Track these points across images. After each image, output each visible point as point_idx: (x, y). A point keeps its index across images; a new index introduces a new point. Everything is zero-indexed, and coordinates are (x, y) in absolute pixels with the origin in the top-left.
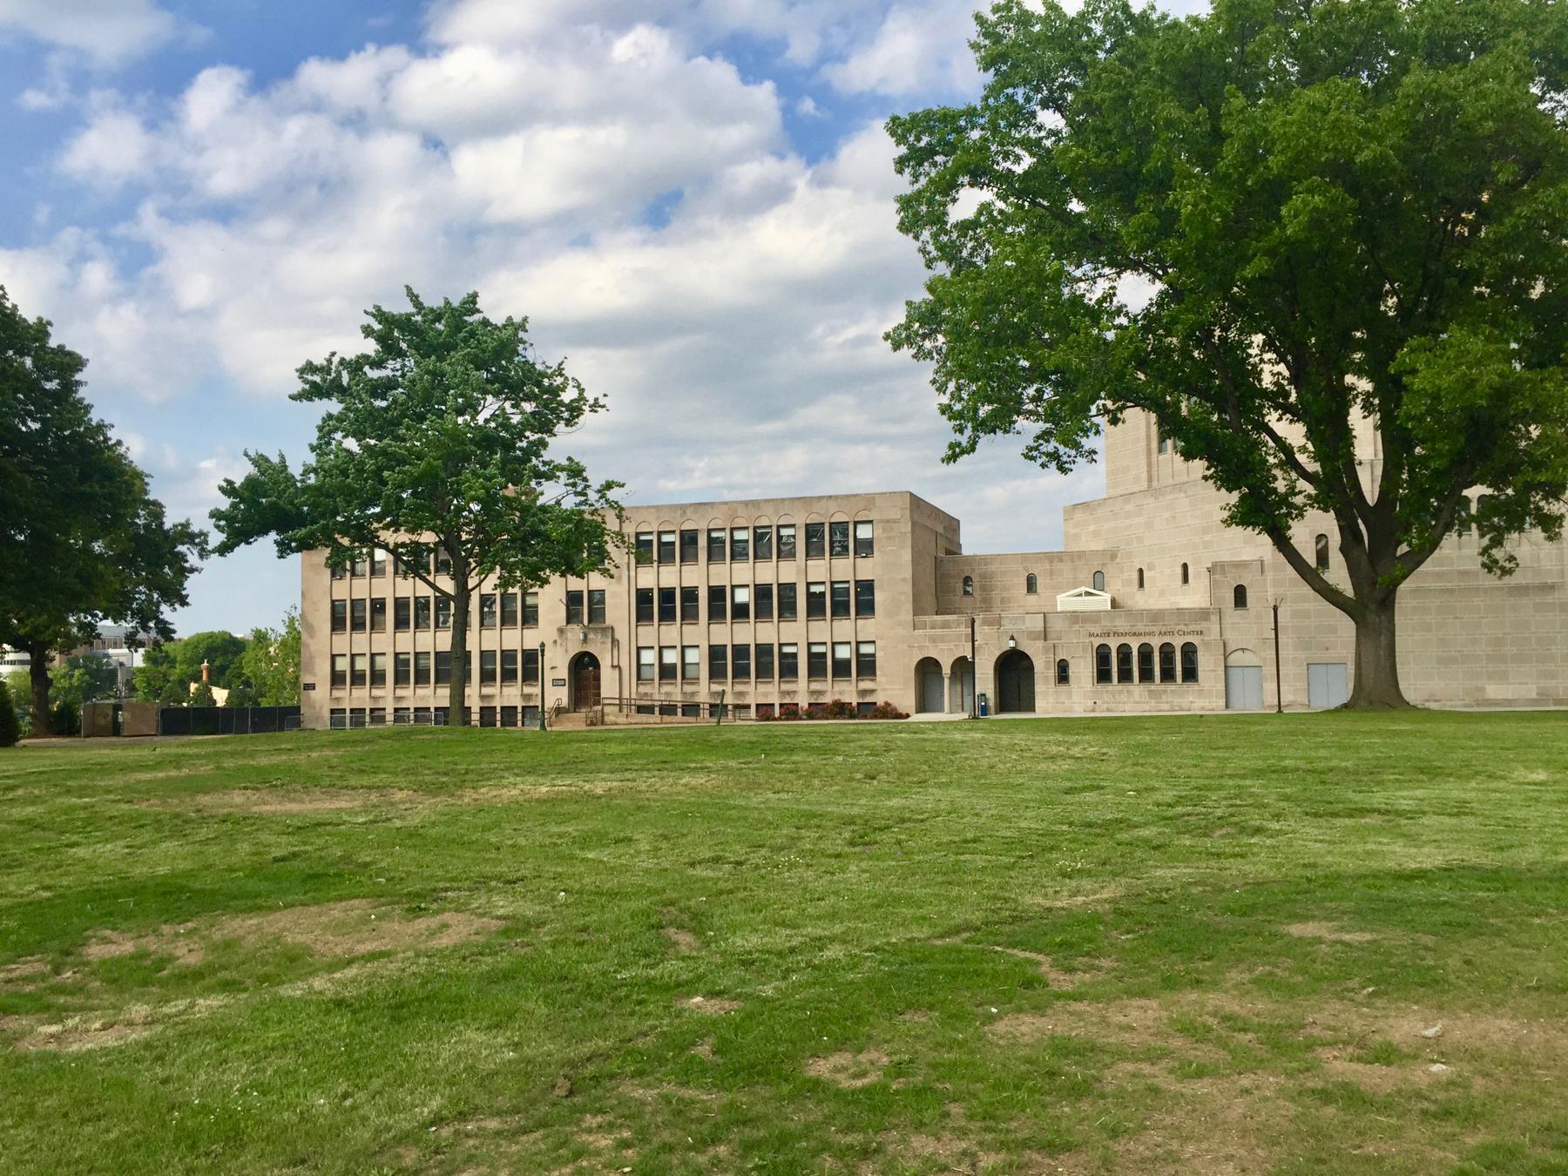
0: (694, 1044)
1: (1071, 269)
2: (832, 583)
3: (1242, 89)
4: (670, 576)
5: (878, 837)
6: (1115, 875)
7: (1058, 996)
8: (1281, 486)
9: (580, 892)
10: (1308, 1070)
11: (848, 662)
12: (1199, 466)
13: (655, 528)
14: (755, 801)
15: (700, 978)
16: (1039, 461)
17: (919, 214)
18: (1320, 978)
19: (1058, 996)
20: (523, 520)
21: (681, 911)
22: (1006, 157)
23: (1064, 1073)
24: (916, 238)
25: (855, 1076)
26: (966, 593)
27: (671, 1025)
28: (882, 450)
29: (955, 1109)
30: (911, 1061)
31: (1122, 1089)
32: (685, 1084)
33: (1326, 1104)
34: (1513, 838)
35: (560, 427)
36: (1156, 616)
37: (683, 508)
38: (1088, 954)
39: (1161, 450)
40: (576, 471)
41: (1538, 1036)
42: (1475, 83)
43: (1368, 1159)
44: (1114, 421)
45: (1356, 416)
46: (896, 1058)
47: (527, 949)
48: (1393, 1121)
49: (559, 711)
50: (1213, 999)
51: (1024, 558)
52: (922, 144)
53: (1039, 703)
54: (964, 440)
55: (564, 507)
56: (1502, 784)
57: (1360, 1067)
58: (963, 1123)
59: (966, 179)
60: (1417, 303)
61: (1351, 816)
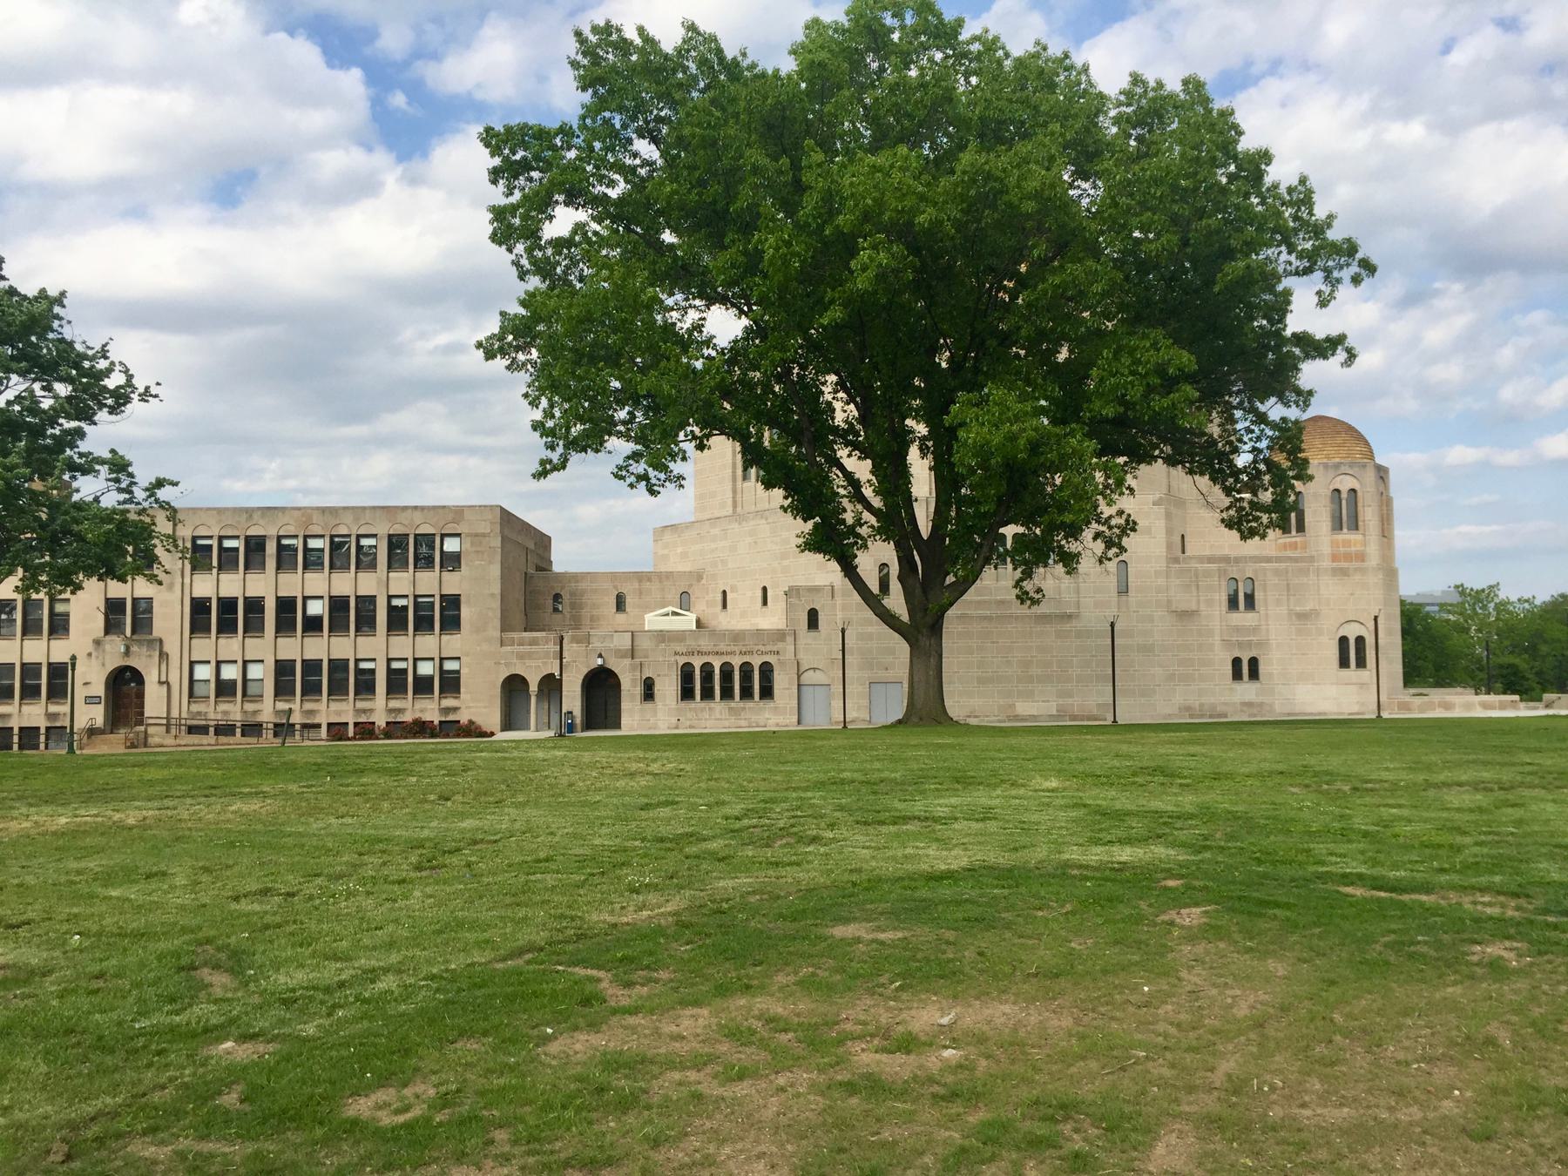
0: (220, 1093)
1: (663, 297)
2: (416, 597)
3: (820, 145)
4: (232, 585)
5: (448, 860)
6: (680, 888)
7: (615, 1012)
8: (849, 517)
9: (99, 934)
10: (838, 1064)
11: (431, 678)
12: (778, 494)
13: (215, 532)
14: (315, 826)
15: (232, 1021)
16: (629, 481)
17: (510, 228)
18: (856, 976)
19: (615, 1012)
20: (52, 519)
21: (219, 949)
22: (601, 178)
23: (610, 1090)
24: (510, 250)
25: (398, 1112)
26: (556, 610)
27: (194, 1074)
28: (473, 462)
29: (500, 1135)
30: (458, 1091)
31: (667, 1098)
32: (202, 1138)
33: (851, 1095)
34: (1024, 840)
35: (103, 415)
36: (737, 636)
37: (249, 512)
38: (648, 967)
39: (745, 478)
40: (119, 466)
41: (1034, 1019)
42: (1019, 166)
43: (883, 1144)
44: (701, 447)
45: (914, 453)
46: (443, 1089)
47: (28, 1002)
48: (908, 1106)
49: (92, 732)
50: (761, 1003)
51: (614, 576)
52: (518, 157)
53: (624, 720)
54: (555, 457)
55: (103, 505)
56: (1022, 791)
57: (884, 1057)
58: (507, 1149)
59: (561, 198)
60: (965, 358)
61: (895, 823)
